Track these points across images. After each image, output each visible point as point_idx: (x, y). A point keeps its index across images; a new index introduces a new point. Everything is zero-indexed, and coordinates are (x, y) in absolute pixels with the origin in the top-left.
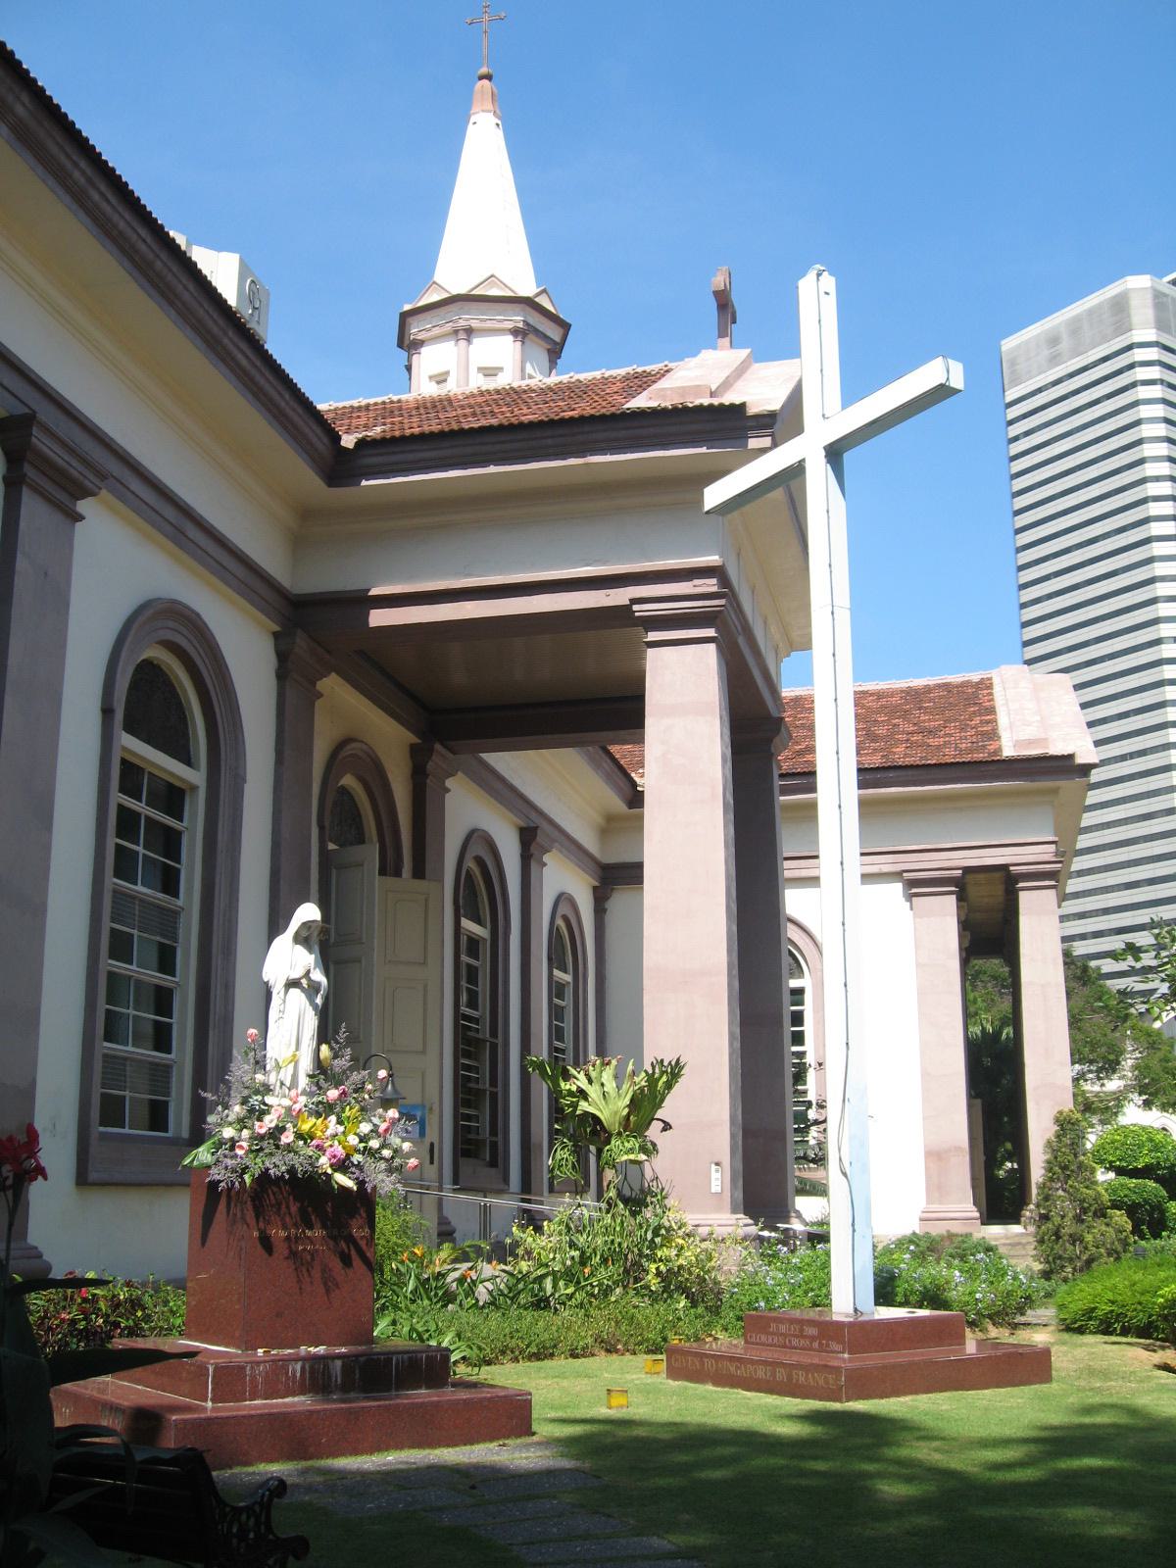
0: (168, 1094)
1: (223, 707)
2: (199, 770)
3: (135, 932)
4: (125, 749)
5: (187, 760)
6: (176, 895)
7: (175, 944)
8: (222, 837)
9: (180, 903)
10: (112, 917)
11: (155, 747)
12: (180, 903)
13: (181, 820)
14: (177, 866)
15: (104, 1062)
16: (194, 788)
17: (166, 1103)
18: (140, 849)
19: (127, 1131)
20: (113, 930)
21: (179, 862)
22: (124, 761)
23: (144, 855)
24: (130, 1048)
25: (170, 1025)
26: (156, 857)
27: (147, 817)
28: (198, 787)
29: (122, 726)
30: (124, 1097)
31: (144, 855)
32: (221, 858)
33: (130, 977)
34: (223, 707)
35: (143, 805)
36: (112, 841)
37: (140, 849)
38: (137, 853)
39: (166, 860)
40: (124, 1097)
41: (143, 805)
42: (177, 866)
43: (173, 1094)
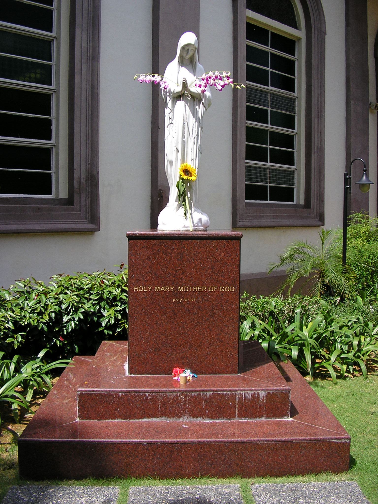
0: (293, 185)
1: (312, 5)
2: (301, 30)
3: (269, 109)
4: (248, 17)
5: (295, 26)
6: (294, 92)
7: (294, 114)
8: (314, 61)
9: (295, 95)
10: (246, 100)
11: (272, 19)
12: (54, 34)
13: (294, 55)
14: (293, 77)
15: (246, 169)
16: (299, 39)
17: (293, 189)
18: (269, 69)
19: (269, 202)
20: (248, 47)
21: (294, 76)
22: (248, 25)
23: (271, 71)
24: (268, 163)
25: (293, 152)
26: (280, 73)
27: (271, 53)
28: (301, 38)
29: (246, 6)
30: (267, 186)
31: (271, 71)
32: (314, 71)
33: (267, 131)
34: (312, 5)
35: (269, 125)
36: (244, 42)
37: (269, 69)
38: (268, 71)
39: (285, 74)
40: (267, 186)
41: (269, 125)
42: (293, 77)
43: (296, 184)
